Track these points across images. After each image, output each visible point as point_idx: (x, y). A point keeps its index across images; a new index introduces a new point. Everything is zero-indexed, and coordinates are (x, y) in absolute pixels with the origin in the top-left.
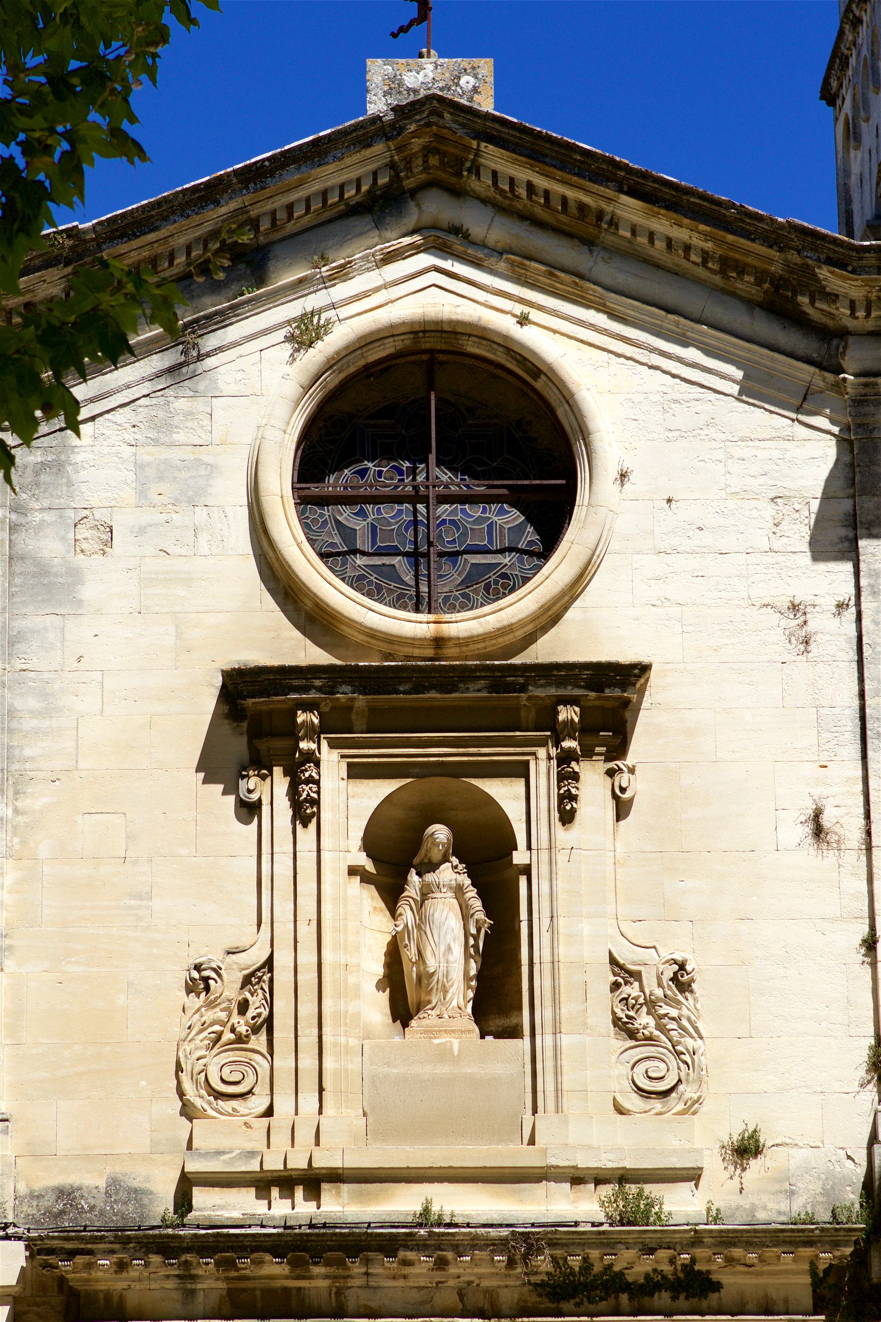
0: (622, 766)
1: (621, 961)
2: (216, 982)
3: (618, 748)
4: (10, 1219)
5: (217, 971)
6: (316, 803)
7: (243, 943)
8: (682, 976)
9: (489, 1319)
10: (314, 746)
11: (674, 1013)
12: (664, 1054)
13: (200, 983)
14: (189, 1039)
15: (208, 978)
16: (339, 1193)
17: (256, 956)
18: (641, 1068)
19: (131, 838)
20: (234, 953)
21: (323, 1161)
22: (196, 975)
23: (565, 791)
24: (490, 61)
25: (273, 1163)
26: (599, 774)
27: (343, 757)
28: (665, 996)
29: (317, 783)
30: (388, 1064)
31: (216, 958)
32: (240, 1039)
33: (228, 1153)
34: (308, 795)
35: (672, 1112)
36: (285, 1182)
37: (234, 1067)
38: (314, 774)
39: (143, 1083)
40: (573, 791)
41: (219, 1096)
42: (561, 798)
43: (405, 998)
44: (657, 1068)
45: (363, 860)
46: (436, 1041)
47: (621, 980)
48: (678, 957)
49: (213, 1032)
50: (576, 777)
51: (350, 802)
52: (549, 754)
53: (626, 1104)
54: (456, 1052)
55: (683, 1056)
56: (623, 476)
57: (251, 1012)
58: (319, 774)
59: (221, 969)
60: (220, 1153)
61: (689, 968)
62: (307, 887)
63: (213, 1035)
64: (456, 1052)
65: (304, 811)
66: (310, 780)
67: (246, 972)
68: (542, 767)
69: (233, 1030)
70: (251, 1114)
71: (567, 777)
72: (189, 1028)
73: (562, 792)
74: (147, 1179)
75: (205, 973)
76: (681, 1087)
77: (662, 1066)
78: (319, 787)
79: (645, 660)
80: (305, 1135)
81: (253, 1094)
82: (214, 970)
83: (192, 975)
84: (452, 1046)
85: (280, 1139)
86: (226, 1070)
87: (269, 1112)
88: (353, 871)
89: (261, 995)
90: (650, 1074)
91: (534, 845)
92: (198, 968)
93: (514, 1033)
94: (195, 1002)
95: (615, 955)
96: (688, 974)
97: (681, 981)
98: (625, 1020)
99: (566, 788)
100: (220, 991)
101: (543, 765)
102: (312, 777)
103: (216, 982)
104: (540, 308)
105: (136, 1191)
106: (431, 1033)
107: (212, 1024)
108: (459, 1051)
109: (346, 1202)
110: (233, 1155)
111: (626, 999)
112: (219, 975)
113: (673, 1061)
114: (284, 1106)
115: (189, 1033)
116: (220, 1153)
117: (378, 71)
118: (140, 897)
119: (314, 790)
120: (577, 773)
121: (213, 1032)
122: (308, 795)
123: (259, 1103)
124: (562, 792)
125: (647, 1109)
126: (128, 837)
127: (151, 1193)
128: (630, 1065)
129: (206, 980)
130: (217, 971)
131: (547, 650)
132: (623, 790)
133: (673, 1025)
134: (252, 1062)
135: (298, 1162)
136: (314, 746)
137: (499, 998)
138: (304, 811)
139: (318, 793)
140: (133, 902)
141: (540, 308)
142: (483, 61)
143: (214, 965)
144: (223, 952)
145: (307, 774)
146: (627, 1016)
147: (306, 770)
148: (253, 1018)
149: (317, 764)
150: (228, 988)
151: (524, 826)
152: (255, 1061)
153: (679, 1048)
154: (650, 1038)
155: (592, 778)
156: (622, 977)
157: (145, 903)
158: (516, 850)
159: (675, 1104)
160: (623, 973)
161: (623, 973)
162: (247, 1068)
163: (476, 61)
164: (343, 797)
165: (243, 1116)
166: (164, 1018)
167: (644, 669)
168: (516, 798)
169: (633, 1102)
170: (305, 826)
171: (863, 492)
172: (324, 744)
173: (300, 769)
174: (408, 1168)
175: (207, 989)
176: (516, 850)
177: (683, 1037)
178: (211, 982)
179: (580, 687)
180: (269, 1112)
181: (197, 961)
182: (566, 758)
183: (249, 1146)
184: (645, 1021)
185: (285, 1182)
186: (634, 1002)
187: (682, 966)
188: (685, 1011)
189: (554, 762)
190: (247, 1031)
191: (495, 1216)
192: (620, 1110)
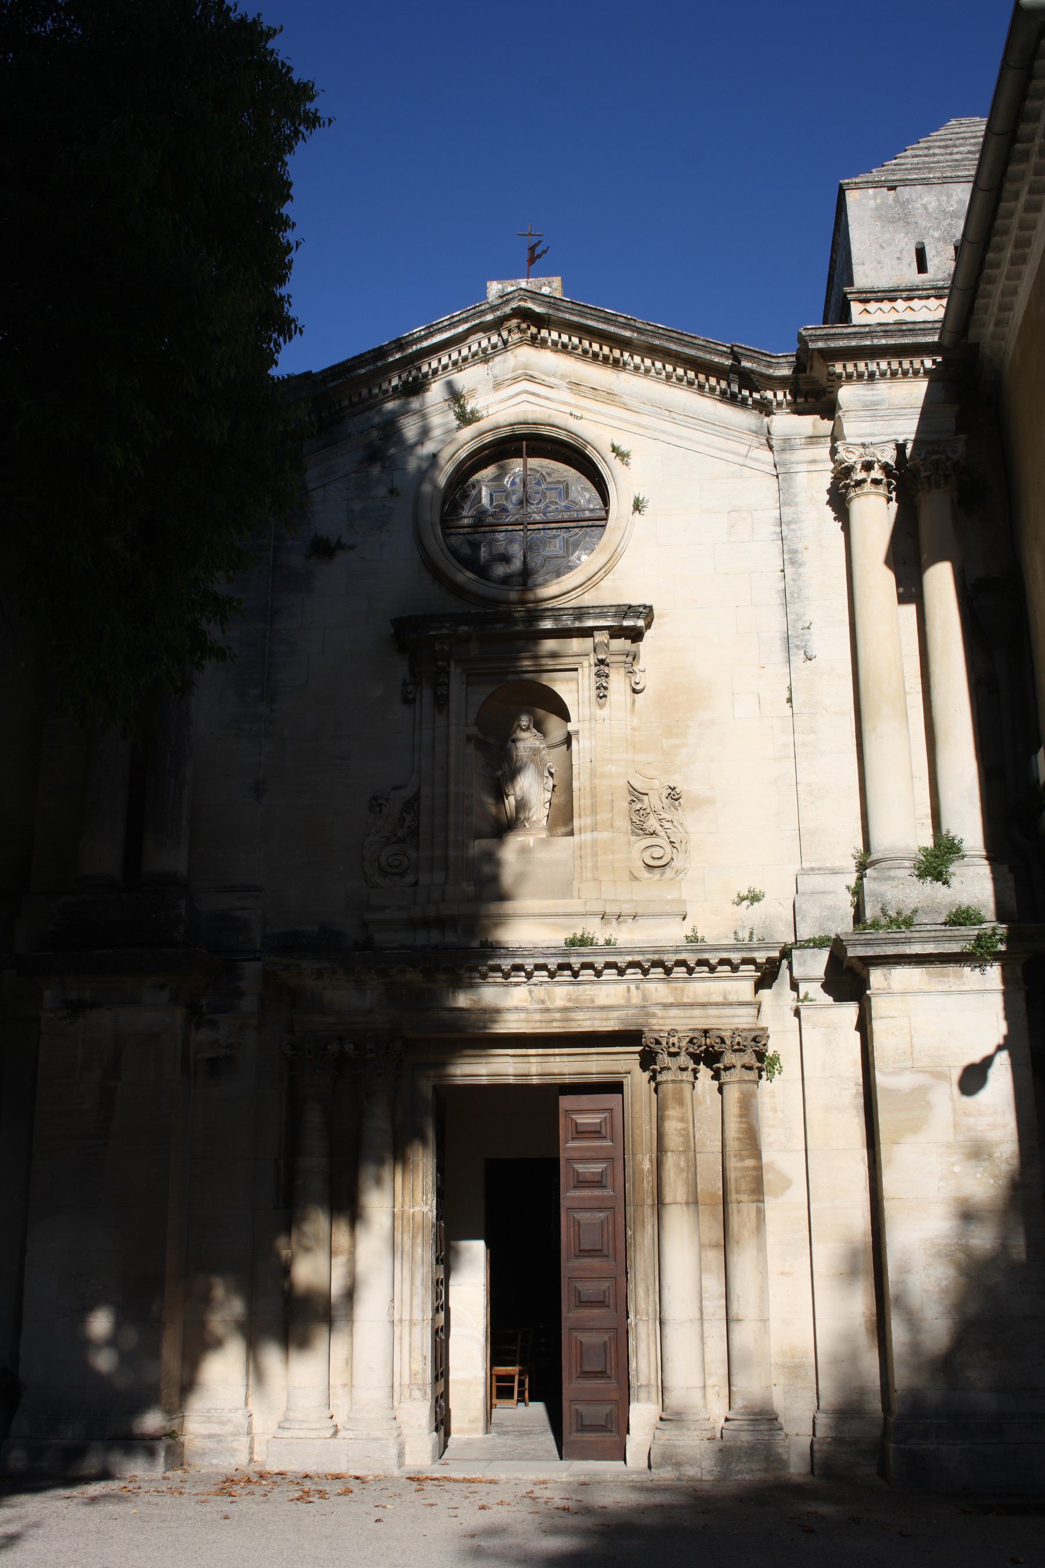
4: (258, 948)
5: (387, 799)
9: (829, 491)
10: (445, 664)
11: (669, 817)
13: (376, 803)
15: (381, 804)
22: (374, 803)
24: (559, 278)
29: (447, 685)
36: (426, 924)
44: (658, 852)
45: (474, 730)
53: (637, 874)
56: (483, 1508)
75: (380, 802)
76: (673, 864)
87: (416, 884)
88: (469, 739)
92: (375, 798)
93: (571, 833)
101: (586, 670)
104: (588, 410)
113: (668, 848)
117: (494, 288)
123: (410, 879)
129: (380, 805)
131: (588, 599)
133: (667, 825)
136: (445, 664)
138: (441, 702)
139: (448, 691)
141: (588, 410)
142: (554, 279)
149: (448, 673)
155: (617, 682)
159: (669, 873)
160: (636, 795)
161: (636, 795)
163: (551, 279)
168: (570, 692)
169: (645, 874)
171: (785, 504)
175: (381, 810)
180: (416, 884)
184: (652, 823)
185: (426, 924)
191: (670, 1365)
192: (634, 878)
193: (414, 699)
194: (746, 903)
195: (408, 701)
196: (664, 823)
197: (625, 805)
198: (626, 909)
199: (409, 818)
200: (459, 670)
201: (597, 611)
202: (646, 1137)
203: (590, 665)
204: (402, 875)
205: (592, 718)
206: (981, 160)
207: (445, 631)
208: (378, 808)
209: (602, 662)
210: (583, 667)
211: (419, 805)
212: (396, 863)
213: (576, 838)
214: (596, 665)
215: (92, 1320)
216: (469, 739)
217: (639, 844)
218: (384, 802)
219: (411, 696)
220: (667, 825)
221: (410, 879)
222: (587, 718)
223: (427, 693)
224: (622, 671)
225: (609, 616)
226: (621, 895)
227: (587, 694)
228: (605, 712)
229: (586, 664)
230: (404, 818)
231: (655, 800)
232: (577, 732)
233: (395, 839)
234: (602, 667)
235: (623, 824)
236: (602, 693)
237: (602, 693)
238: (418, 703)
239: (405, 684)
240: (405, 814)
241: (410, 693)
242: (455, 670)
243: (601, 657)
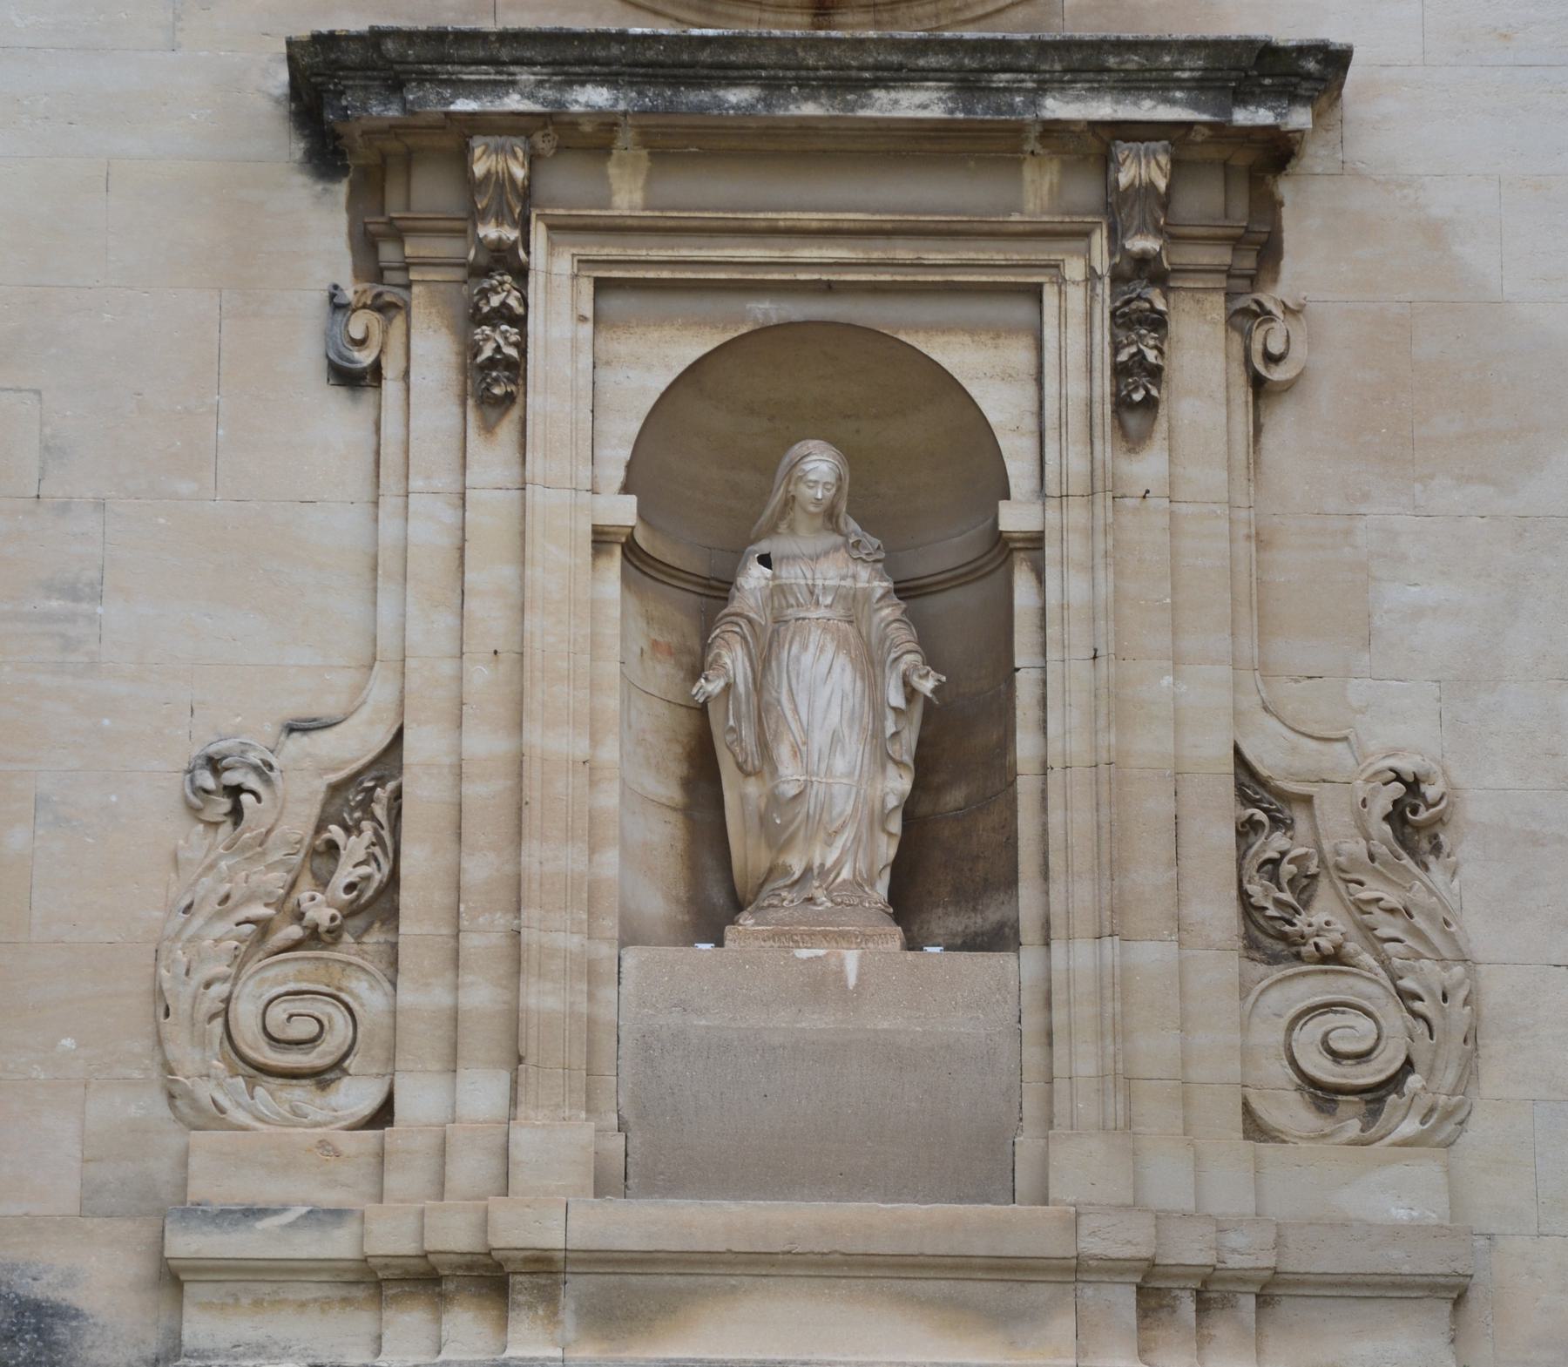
0: (1270, 305)
1: (1263, 771)
2: (259, 799)
3: (1262, 249)
5: (263, 770)
6: (516, 369)
7: (325, 707)
8: (1415, 811)
10: (512, 234)
11: (1392, 898)
12: (1369, 998)
13: (221, 789)
14: (185, 936)
16: (555, 1314)
17: (353, 745)
18: (1314, 1029)
19: (51, 450)
20: (305, 730)
21: (525, 1227)
22: (207, 780)
23: (1132, 356)
25: (392, 1238)
26: (1214, 323)
27: (585, 262)
28: (1372, 858)
29: (520, 322)
30: (684, 1007)
31: (247, 727)
32: (314, 937)
33: (276, 1212)
34: (498, 349)
35: (1388, 1140)
37: (298, 1006)
38: (513, 302)
39: (68, 1043)
40: (1151, 356)
41: (1329, 1007)
42: (1120, 371)
43: (718, 893)
44: (1352, 1032)
45: (623, 511)
46: (803, 953)
47: (1260, 816)
48: (1407, 765)
49: (247, 921)
50: (1158, 323)
51: (600, 374)
52: (1092, 269)
53: (1270, 1114)
54: (852, 981)
55: (1417, 1005)
57: (346, 873)
58: (524, 302)
59: (271, 768)
60: (253, 1213)
61: (1431, 792)
62: (488, 574)
63: (248, 928)
64: (852, 981)
65: (495, 385)
66: (504, 315)
67: (334, 777)
68: (1076, 320)
69: (299, 917)
70: (337, 1119)
71: (1136, 320)
72: (188, 909)
73: (1123, 357)
74: (70, 1279)
75: (231, 778)
76: (1414, 1082)
77: (1366, 1024)
78: (524, 334)
79: (1336, 36)
80: (471, 1168)
81: (345, 1072)
82: (256, 768)
83: (199, 782)
84: (842, 965)
85: (406, 1181)
86: (278, 1013)
88: (601, 539)
89: (368, 835)
90: (1335, 1045)
91: (1052, 487)
92: (214, 764)
93: (1001, 938)
94: (196, 842)
95: (1249, 754)
96: (1429, 806)
97: (1414, 819)
98: (1272, 912)
99: (1133, 349)
100: (269, 820)
101: (1076, 297)
102: (510, 308)
103: (259, 799)
105: (37, 1308)
106: (787, 937)
107: (250, 899)
108: (860, 977)
109: (571, 1335)
110: (289, 1217)
111: (1275, 863)
112: (268, 781)
113: (1394, 1017)
114: (419, 1101)
115: (185, 924)
116: (253, 1213)
118: (72, 592)
119: (513, 338)
120: (1160, 313)
121: (247, 921)
122: (498, 349)
123: (356, 1095)
124: (1123, 357)
125: (1327, 1130)
126: (47, 448)
127: (78, 1314)
128: (1284, 1023)
129: (235, 791)
130: (263, 770)
132: (1272, 359)
133: (1388, 927)
134: (343, 996)
135: (454, 1235)
136: (512, 234)
137: (951, 858)
138: (495, 385)
139: (522, 347)
140: (54, 604)
143: (253, 757)
144: (278, 729)
145: (495, 301)
146: (1278, 903)
147: (494, 290)
148: (350, 887)
149: (522, 274)
150: (290, 809)
151: (1030, 443)
152: (351, 993)
153: (1408, 983)
154: (1334, 958)
155: (1199, 348)
156: (1265, 810)
157: (85, 607)
158: (1007, 497)
160: (1260, 799)
161: (1260, 799)
162: (330, 1009)
164: (586, 360)
165: (317, 1125)
166: (130, 877)
167: (1336, 60)
168: (1007, 377)
169: (1289, 1111)
170: (488, 428)
172: (539, 233)
173: (490, 296)
174: (730, 1251)
175: (237, 813)
176: (1007, 497)
177: (1419, 956)
178: (246, 799)
179: (1173, 102)
180: (383, 1115)
181: (212, 750)
182: (1138, 272)
183: (331, 1198)
184: (1324, 917)
186: (1293, 868)
187: (1413, 786)
188: (1419, 895)
189: (1104, 289)
190: (333, 919)
192: (1255, 1128)
193: (376, 370)
194: (1184, 935)
195: (353, 378)
196: (1377, 917)
197: (1226, 836)
198: (1247, 1252)
199: (354, 847)
200: (564, 264)
201: (1134, 61)
202: (462, 52)
203: (1092, 276)
204: (322, 1077)
205: (1102, 488)
206: (1134, 140)
207: (513, 102)
208: (225, 804)
209: (1146, 269)
210: (1061, 282)
211: (398, 795)
212: (310, 1029)
213: (1029, 959)
214: (1117, 278)
215: (1108, 98)
216: (601, 539)
217: (1274, 996)
218: (252, 781)
219: (364, 358)
220: (1388, 927)
221: (356, 1095)
222: (1077, 485)
223: (430, 351)
224: (1216, 307)
225: (1180, 84)
226: (1216, 1199)
227: (1076, 389)
228: (1148, 467)
229: (1074, 269)
230: (332, 848)
231: (1341, 827)
232: (1036, 542)
233: (295, 932)
234: (1139, 287)
235: (1218, 915)
236: (1136, 395)
237: (1136, 395)
238: (391, 386)
239: (337, 306)
240: (335, 832)
241: (361, 343)
242: (555, 272)
243: (1142, 243)
